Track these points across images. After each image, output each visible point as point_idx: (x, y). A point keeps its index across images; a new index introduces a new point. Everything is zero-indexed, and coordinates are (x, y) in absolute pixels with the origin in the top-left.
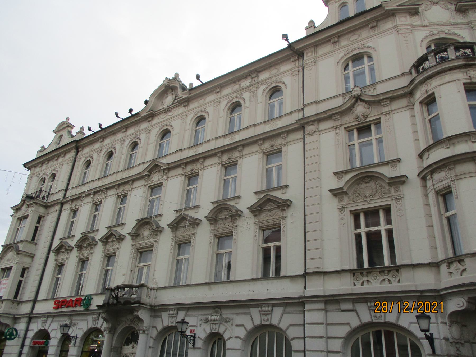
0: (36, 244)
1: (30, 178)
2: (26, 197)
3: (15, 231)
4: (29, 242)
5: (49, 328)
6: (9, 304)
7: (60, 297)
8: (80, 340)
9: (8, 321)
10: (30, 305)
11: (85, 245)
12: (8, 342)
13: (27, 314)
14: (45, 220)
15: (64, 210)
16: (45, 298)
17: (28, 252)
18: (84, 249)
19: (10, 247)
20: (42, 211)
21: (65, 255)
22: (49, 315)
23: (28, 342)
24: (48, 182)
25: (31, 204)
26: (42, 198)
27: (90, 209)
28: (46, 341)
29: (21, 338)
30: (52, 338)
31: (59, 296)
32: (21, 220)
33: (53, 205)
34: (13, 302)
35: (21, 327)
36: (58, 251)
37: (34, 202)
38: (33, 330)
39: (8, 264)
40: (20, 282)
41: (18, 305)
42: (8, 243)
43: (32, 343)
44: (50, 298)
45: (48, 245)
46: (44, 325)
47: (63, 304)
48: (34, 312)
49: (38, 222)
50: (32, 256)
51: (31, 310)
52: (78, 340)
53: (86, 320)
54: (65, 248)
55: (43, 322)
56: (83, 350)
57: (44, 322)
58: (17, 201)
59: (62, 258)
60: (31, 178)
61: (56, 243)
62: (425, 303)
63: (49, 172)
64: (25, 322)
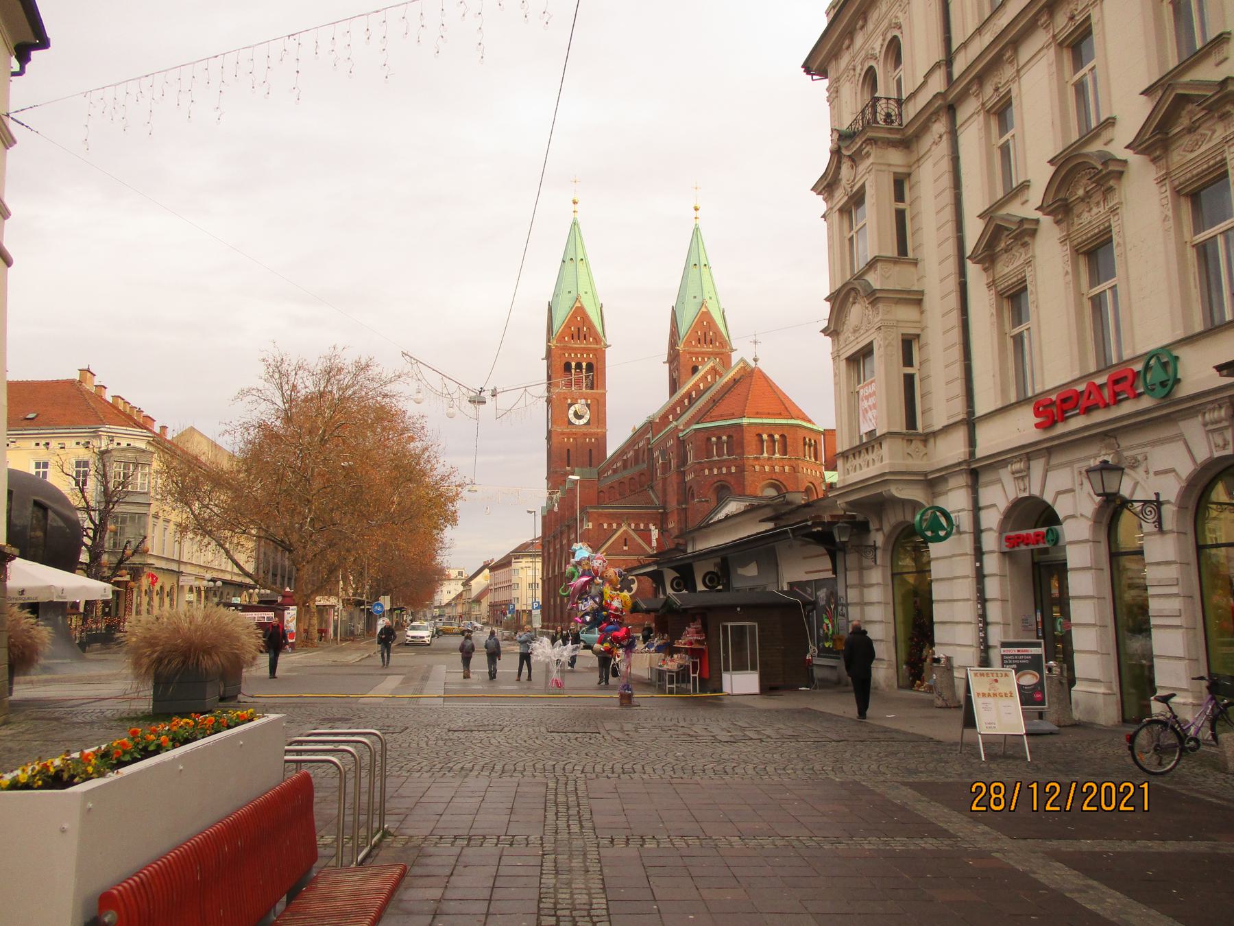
0: (915, 263)
1: (834, 95)
2: (839, 139)
3: (845, 245)
4: (894, 261)
5: (1042, 491)
6: (899, 445)
7: (1047, 388)
8: (1175, 509)
9: (915, 494)
10: (960, 436)
11: (1081, 192)
12: (935, 549)
13: (959, 464)
14: (917, 183)
15: (961, 126)
16: (999, 405)
17: (898, 288)
18: (1077, 210)
19: (848, 294)
20: (896, 158)
21: (1018, 254)
22: (1029, 450)
23: (990, 542)
24: (886, 72)
25: (860, 150)
26: (885, 121)
27: (1054, 69)
28: (1048, 531)
29: (965, 532)
30: (1066, 518)
31: (1043, 384)
32: (851, 211)
33: (924, 128)
34: (908, 440)
35: (955, 500)
36: (989, 253)
37: (863, 139)
38: (994, 505)
39: (859, 340)
40: (909, 380)
41: (925, 446)
42: (838, 285)
43: (1004, 543)
44: (1013, 400)
45: (950, 248)
46: (1024, 485)
47: (1065, 406)
48: (980, 453)
49: (899, 196)
50: (916, 299)
51: (967, 450)
52: (1169, 512)
53: (1180, 437)
54: (1006, 233)
55: (1017, 475)
56: (1201, 543)
57: (1021, 476)
58: (820, 161)
59: (1011, 267)
60: (837, 92)
61: (974, 230)
62: (1101, 786)
63: (878, 45)
64: (962, 487)
